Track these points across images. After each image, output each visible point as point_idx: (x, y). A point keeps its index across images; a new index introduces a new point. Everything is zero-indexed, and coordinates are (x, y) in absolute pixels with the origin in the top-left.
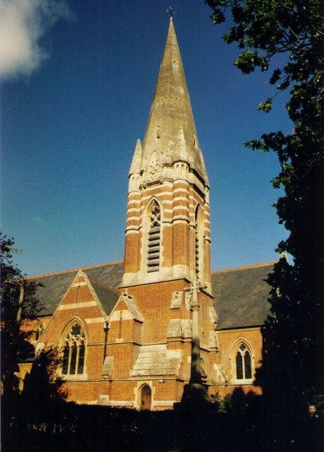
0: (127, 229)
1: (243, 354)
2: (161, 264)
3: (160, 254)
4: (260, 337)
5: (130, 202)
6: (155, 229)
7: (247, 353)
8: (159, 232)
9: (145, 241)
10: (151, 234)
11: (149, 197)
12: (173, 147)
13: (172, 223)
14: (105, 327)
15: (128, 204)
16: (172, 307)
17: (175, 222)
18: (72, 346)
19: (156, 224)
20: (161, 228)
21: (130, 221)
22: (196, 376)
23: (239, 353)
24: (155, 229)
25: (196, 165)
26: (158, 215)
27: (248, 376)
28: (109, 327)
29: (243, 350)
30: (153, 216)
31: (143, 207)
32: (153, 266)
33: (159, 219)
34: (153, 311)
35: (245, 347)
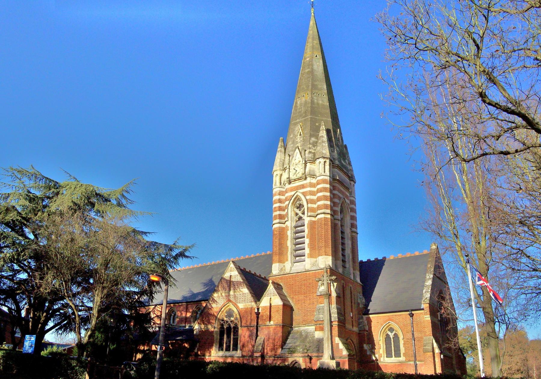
0: (273, 223)
1: (391, 335)
2: (306, 255)
3: (306, 246)
4: (411, 373)
5: (275, 205)
6: (300, 223)
7: (395, 334)
8: (304, 225)
9: (289, 234)
10: (296, 227)
11: (293, 193)
12: (315, 144)
13: (316, 217)
14: (256, 311)
15: (274, 199)
16: (319, 294)
17: (319, 216)
18: (234, 327)
19: (300, 218)
20: (306, 223)
21: (276, 216)
22: (312, 102)
23: (387, 335)
24: (300, 223)
25: (340, 162)
26: (302, 209)
27: (398, 355)
28: (260, 311)
29: (392, 333)
30: (297, 211)
31: (287, 202)
32: (298, 256)
33: (303, 213)
34: (301, 297)
35: (393, 330)
